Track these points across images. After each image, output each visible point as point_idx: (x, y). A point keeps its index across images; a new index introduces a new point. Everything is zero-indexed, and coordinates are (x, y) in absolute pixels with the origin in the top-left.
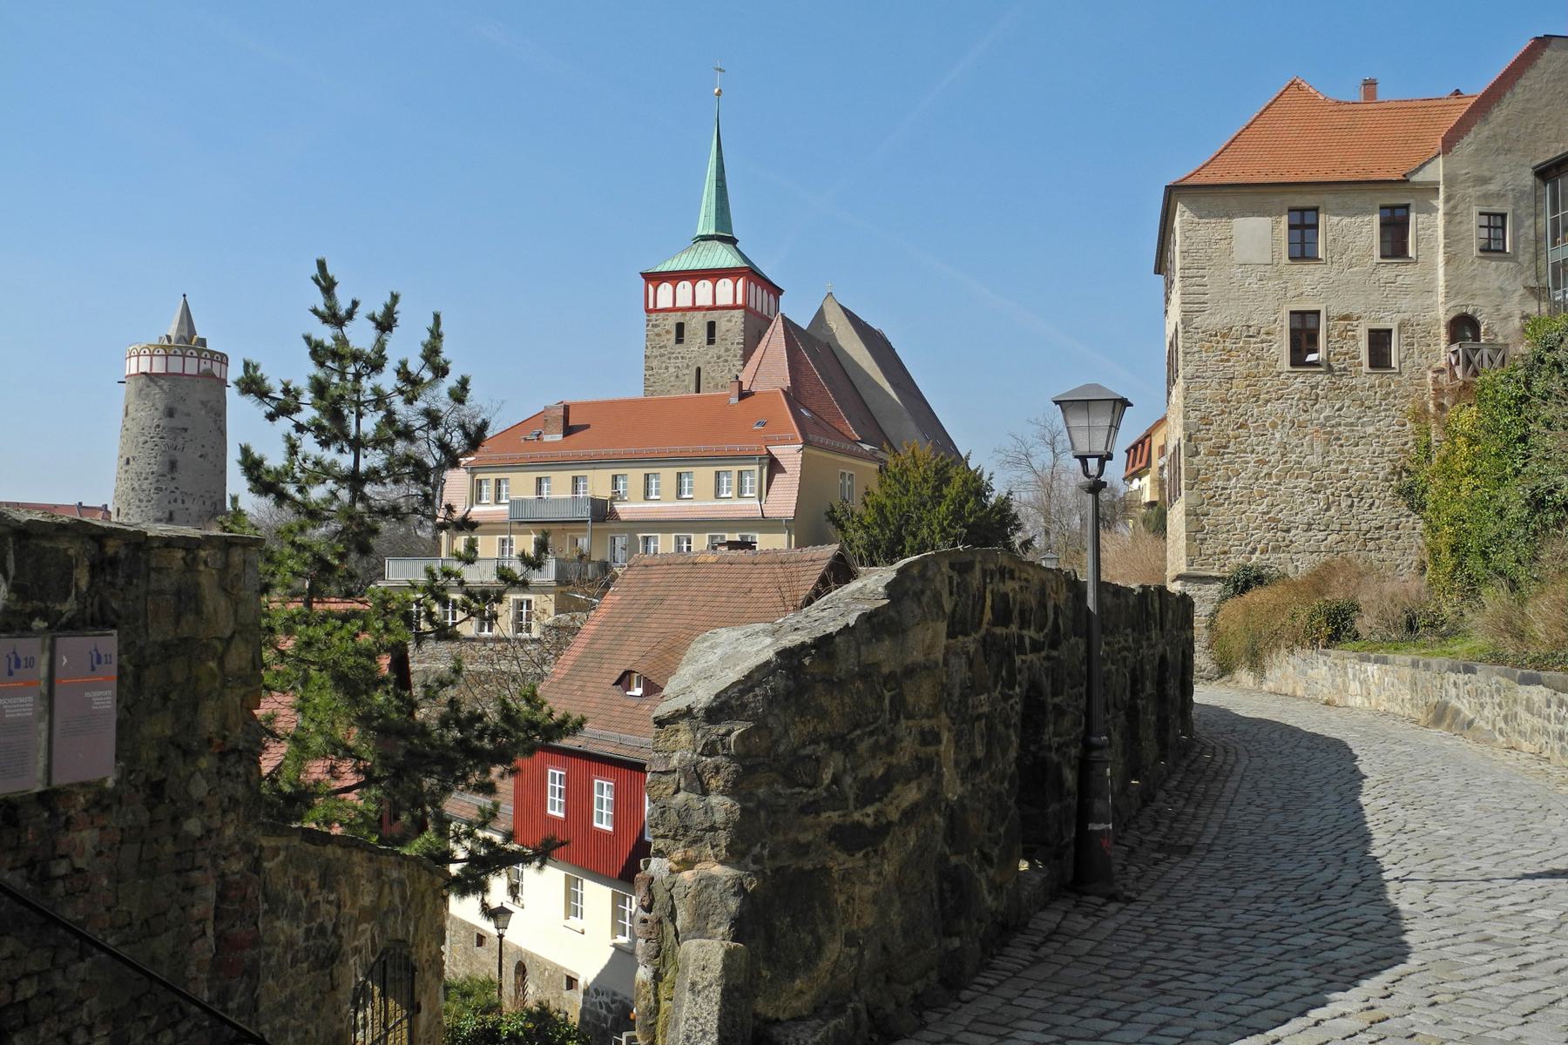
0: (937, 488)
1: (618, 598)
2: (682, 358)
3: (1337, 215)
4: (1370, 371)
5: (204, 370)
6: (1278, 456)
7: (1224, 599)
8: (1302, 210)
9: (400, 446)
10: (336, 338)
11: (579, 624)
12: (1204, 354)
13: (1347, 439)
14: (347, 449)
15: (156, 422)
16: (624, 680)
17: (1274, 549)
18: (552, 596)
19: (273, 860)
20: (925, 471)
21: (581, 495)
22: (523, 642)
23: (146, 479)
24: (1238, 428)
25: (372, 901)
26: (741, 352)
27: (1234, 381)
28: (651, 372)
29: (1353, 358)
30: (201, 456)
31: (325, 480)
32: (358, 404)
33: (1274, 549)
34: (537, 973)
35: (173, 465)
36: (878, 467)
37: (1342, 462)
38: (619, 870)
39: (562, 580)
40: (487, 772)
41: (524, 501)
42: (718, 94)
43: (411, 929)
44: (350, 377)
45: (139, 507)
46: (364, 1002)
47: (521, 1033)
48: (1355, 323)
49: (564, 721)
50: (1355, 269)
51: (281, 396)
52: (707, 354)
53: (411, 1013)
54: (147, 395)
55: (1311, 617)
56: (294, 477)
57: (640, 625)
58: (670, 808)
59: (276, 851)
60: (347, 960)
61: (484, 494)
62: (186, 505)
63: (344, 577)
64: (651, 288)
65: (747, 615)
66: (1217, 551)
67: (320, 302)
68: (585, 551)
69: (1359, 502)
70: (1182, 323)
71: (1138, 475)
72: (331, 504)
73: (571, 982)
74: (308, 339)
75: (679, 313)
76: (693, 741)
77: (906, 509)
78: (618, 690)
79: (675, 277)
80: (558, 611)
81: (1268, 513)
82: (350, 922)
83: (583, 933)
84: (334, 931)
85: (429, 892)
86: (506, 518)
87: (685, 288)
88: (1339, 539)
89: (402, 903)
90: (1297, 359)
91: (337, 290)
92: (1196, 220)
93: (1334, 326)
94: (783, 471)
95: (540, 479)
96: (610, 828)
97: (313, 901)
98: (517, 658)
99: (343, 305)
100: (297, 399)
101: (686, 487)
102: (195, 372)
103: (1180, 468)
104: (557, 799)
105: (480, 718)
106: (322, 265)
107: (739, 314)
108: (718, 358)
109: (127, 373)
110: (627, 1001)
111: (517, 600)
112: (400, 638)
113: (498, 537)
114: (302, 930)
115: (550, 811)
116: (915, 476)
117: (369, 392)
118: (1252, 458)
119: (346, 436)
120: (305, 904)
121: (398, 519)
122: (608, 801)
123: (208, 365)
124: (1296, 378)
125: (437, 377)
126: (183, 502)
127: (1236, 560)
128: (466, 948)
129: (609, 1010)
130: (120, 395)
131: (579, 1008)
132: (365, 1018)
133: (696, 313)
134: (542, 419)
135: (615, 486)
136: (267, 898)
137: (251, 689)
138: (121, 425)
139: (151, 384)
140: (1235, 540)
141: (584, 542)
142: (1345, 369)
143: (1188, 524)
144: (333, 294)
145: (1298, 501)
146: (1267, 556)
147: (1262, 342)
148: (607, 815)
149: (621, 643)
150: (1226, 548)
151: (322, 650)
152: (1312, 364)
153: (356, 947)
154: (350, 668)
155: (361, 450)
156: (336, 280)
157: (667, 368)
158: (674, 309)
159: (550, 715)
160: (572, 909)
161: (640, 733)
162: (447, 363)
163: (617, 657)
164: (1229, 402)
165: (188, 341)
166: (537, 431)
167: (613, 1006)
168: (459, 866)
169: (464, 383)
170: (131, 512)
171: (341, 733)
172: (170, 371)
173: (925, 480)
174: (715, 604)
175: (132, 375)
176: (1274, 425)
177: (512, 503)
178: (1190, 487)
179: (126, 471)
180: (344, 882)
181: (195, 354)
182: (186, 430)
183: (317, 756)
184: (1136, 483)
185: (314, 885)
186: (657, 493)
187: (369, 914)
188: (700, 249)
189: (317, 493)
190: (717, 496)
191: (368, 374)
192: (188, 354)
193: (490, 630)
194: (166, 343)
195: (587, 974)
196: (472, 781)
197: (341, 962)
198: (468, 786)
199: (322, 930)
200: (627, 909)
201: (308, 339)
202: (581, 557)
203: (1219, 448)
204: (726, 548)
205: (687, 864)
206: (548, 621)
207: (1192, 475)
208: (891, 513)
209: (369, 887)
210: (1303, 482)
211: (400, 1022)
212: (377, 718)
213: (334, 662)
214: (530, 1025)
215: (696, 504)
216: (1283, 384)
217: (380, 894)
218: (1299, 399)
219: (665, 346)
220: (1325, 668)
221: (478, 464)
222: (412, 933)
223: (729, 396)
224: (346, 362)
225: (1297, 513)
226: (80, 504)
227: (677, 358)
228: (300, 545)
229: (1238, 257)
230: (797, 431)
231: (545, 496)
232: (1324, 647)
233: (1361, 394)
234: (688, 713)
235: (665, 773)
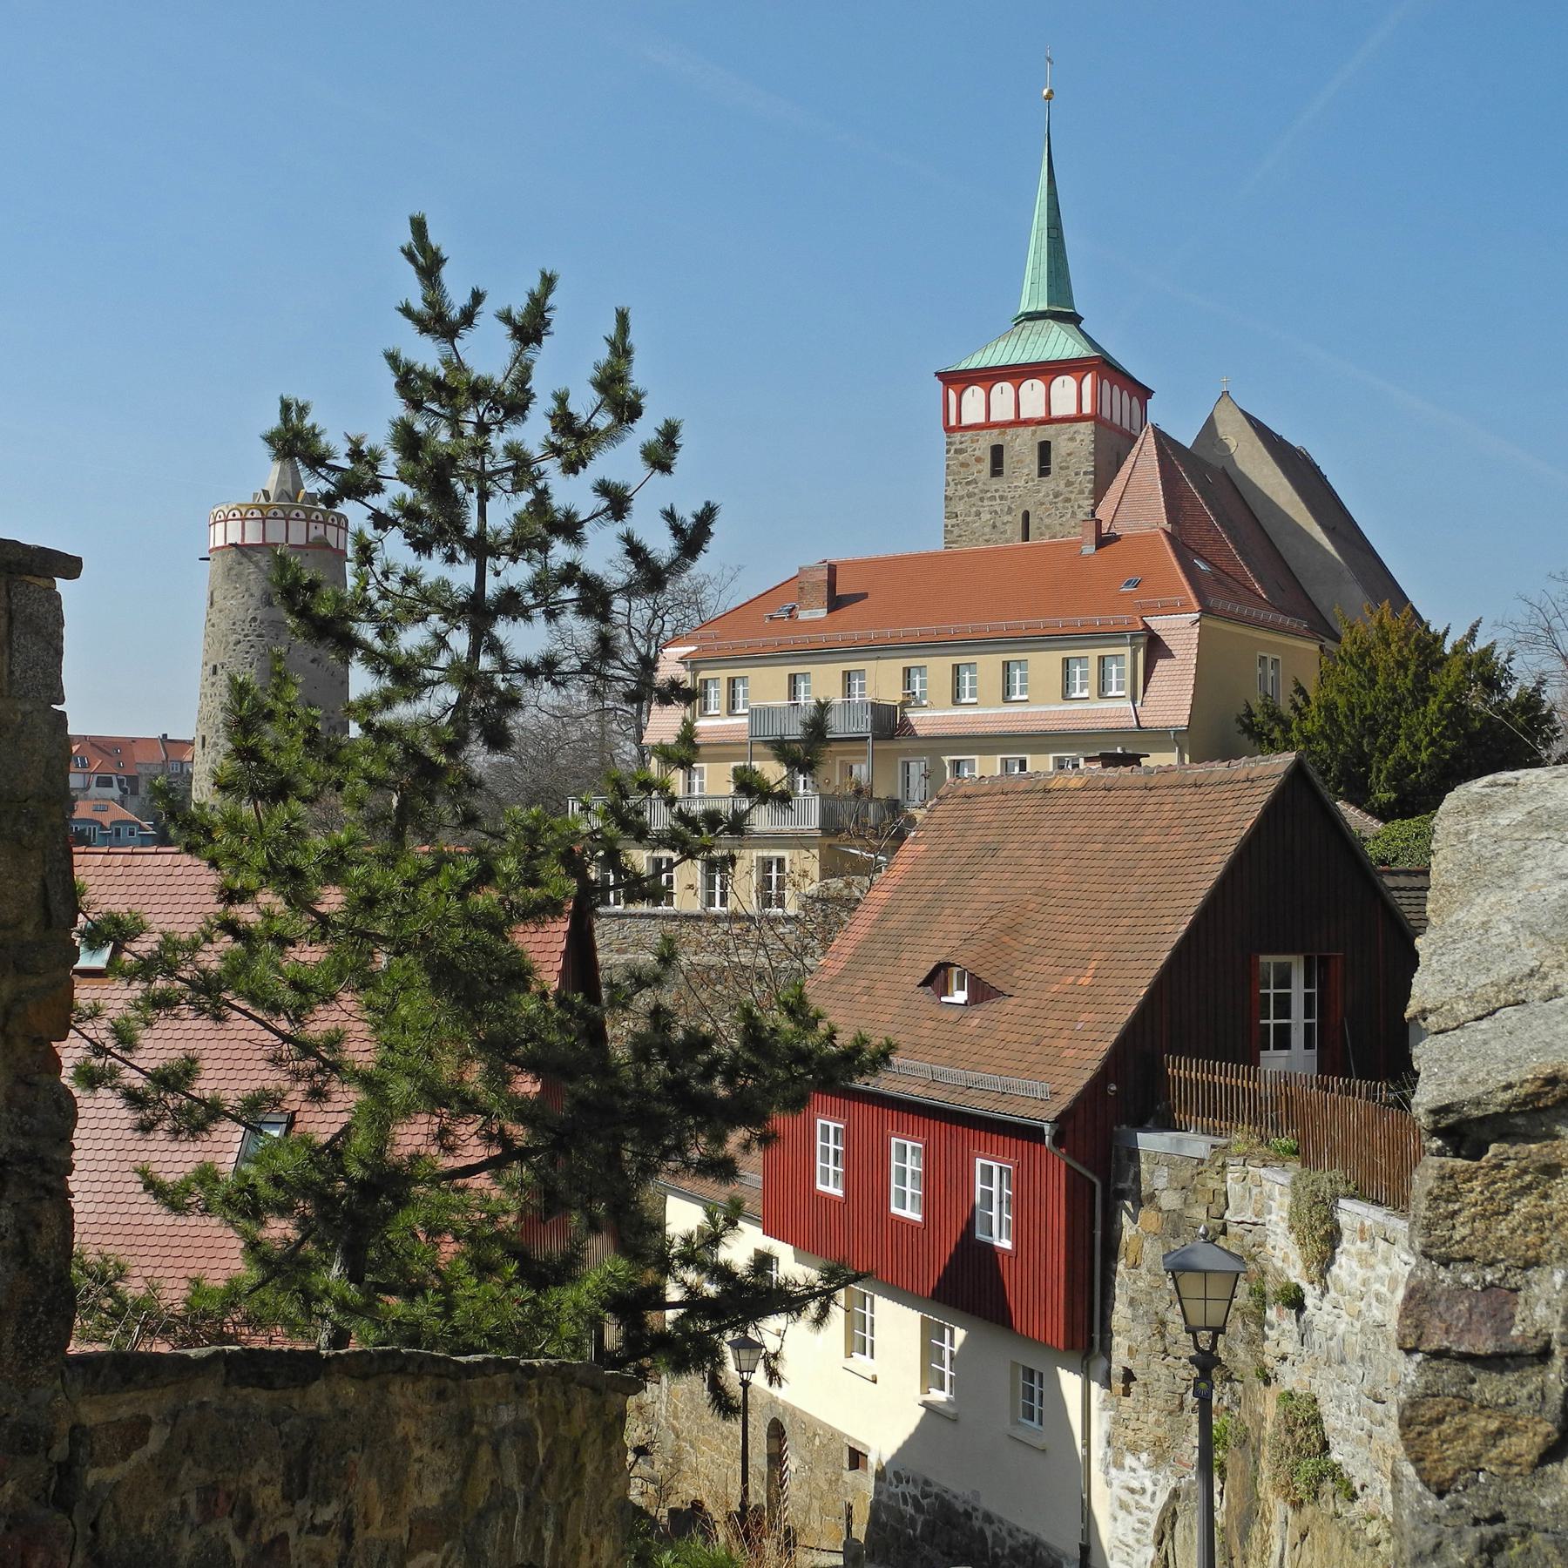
0: (1420, 678)
1: (923, 847)
2: (1001, 498)
5: (315, 538)
9: (561, 552)
10: (446, 363)
11: (857, 894)
14: (462, 555)
16: (937, 978)
18: (816, 852)
19: (125, 1456)
20: (1400, 651)
21: (857, 699)
22: (775, 920)
25: (444, 1495)
30: (313, 661)
31: (428, 614)
32: (483, 476)
34: (802, 1440)
38: (933, 1282)
39: (830, 826)
40: (720, 1139)
42: (1048, 98)
43: (548, 1535)
44: (469, 430)
51: (346, 463)
54: (239, 575)
56: (372, 610)
57: (959, 889)
58: (1525, 1530)
59: (138, 1430)
63: (458, 787)
64: (952, 395)
65: (1139, 872)
67: (414, 293)
72: (436, 656)
73: (856, 1458)
74: (392, 358)
75: (996, 431)
77: (1369, 710)
79: (988, 377)
80: (826, 873)
83: (875, 1382)
85: (592, 1435)
86: (745, 736)
87: (1003, 392)
89: (524, 1479)
91: (445, 273)
94: (1169, 655)
96: (918, 1217)
97: (266, 1538)
98: (765, 946)
99: (457, 299)
100: (374, 468)
101: (1018, 684)
102: (303, 542)
104: (831, 1167)
105: (705, 1043)
106: (419, 226)
107: (1086, 428)
108: (1056, 497)
110: (947, 1496)
111: (763, 858)
116: (1384, 658)
117: (500, 456)
119: (460, 528)
121: (555, 683)
122: (913, 1173)
123: (321, 531)
125: (620, 421)
128: (692, 1393)
129: (918, 1507)
130: (203, 577)
131: (869, 1501)
133: (1021, 430)
134: (795, 587)
137: (33, 981)
139: (244, 560)
141: (862, 771)
148: (913, 1196)
154: (458, 950)
155: (489, 560)
156: (444, 253)
157: (978, 514)
158: (988, 425)
159: (831, 1037)
160: (857, 1343)
161: (964, 1064)
162: (639, 396)
163: (922, 941)
166: (789, 605)
167: (925, 1502)
168: (670, 1315)
169: (670, 434)
171: (448, 1072)
174: (1084, 855)
175: (218, 548)
177: (753, 714)
179: (213, 684)
181: (302, 516)
185: (268, 1497)
186: (973, 693)
188: (1025, 333)
189: (412, 639)
191: (499, 423)
193: (723, 902)
194: (263, 501)
195: (883, 1444)
196: (695, 1155)
198: (688, 1165)
200: (946, 1346)
201: (392, 358)
202: (859, 792)
206: (811, 888)
208: (1346, 716)
209: (440, 1461)
212: (525, 1042)
215: (1031, 710)
219: (975, 482)
222: (549, 1543)
223: (1080, 542)
224: (461, 400)
226: (165, 736)
228: (382, 729)
235: (1498, 1362)
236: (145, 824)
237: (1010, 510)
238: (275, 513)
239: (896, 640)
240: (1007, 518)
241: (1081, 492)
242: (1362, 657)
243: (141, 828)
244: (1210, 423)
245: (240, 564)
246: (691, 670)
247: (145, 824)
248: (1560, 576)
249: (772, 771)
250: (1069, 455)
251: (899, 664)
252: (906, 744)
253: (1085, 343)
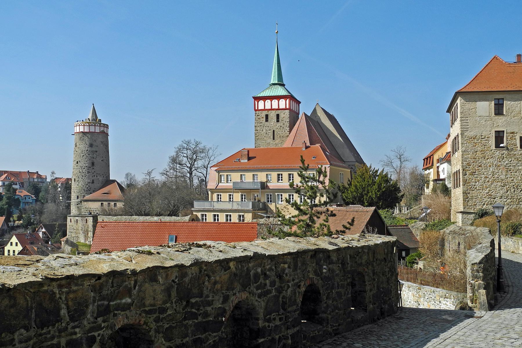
2: (268, 127)
3: (510, 101)
4: (520, 149)
5: (102, 131)
6: (491, 176)
7: (475, 219)
8: (498, 99)
12: (468, 144)
13: (513, 170)
17: (490, 204)
23: (84, 169)
24: (479, 167)
27: (477, 152)
28: (257, 132)
29: (515, 145)
30: (102, 161)
33: (490, 204)
35: (93, 164)
36: (350, 171)
37: (511, 178)
42: (277, 33)
45: (82, 178)
48: (515, 135)
50: (516, 118)
52: (277, 126)
54: (83, 139)
55: (507, 228)
61: (222, 179)
62: (98, 178)
66: (473, 204)
69: (517, 190)
70: (461, 134)
71: (429, 168)
75: (266, 111)
76: (477, 266)
79: (264, 98)
80: (253, 218)
81: (488, 193)
86: (232, 187)
87: (268, 102)
88: (511, 201)
90: (497, 146)
92: (465, 102)
93: (509, 135)
102: (99, 132)
103: (459, 178)
107: (287, 112)
109: (75, 132)
111: (239, 215)
113: (228, 194)
118: (482, 176)
124: (497, 152)
126: (97, 177)
127: (478, 207)
130: (73, 140)
139: (84, 136)
140: (478, 201)
142: (512, 149)
143: (463, 196)
145: (498, 189)
146: (488, 206)
147: (486, 140)
150: (475, 204)
152: (502, 147)
157: (263, 130)
158: (265, 110)
164: (476, 159)
165: (95, 121)
166: (238, 158)
170: (79, 180)
172: (90, 131)
176: (490, 166)
178: (464, 185)
181: (99, 125)
182: (97, 151)
184: (427, 172)
188: (273, 88)
192: (96, 125)
194: (88, 121)
203: (473, 173)
205: (477, 281)
207: (465, 181)
208: (359, 188)
210: (499, 184)
216: (493, 153)
218: (498, 158)
219: (262, 123)
220: (511, 242)
225: (497, 193)
226: (28, 171)
227: (266, 127)
229: (478, 114)
230: (327, 160)
232: (511, 236)
233: (517, 156)
234: (476, 263)
236: (32, 196)
237: (270, 130)
238: (92, 124)
239: (264, 168)
240: (269, 132)
241: (286, 126)
243: (32, 197)
244: (315, 110)
245: (83, 136)
246: (218, 173)
247: (32, 196)
248: (393, 151)
249: (348, 226)
250: (284, 117)
251: (265, 173)
252: (267, 190)
253: (287, 91)
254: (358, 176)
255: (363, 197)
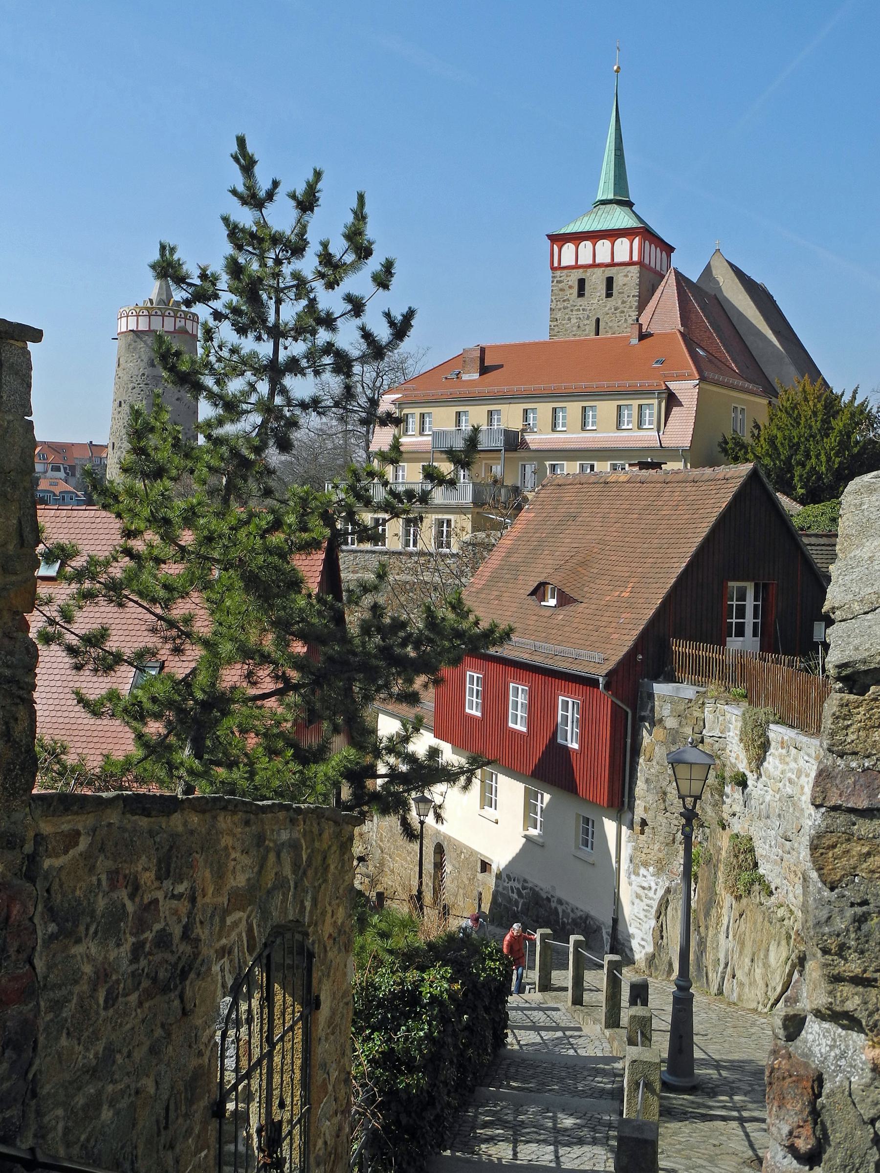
1: (533, 515)
2: (583, 310)
10: (257, 223)
11: (493, 541)
14: (265, 337)
15: (142, 371)
16: (539, 591)
18: (470, 516)
19: (66, 852)
20: (815, 406)
25: (249, 880)
26: (636, 304)
28: (555, 323)
30: (177, 399)
31: (245, 371)
32: (278, 290)
38: (532, 767)
39: (478, 502)
40: (410, 681)
41: (444, 433)
42: (617, 71)
43: (308, 904)
46: (249, 990)
47: (445, 996)
49: (491, 631)
51: (197, 282)
53: (306, 1012)
54: (135, 349)
56: (212, 369)
57: (553, 540)
59: (73, 838)
60: (210, 969)
64: (556, 248)
67: (239, 182)
68: (499, 476)
73: (485, 866)
74: (226, 220)
75: (581, 270)
77: (796, 440)
78: (532, 601)
79: (577, 238)
80: (475, 529)
82: (212, 916)
84: (186, 935)
85: (334, 848)
87: (586, 247)
89: (294, 872)
91: (257, 169)
95: (459, 413)
96: (524, 729)
97: (146, 901)
99: (263, 185)
100: (214, 285)
101: (590, 420)
102: (172, 329)
104: (475, 699)
105: (403, 625)
106: (241, 142)
107: (635, 269)
110: (537, 889)
111: (439, 519)
112: (314, 535)
114: (126, 948)
115: (468, 710)
116: (806, 410)
117: (288, 278)
119: (264, 321)
120: (130, 907)
121: (319, 413)
123: (183, 323)
125: (360, 258)
128: (391, 827)
132: (249, 1011)
134: (461, 360)
135: (526, 419)
136: (52, 913)
138: (114, 374)
139: (138, 340)
141: (497, 469)
144: (252, 173)
148: (522, 717)
149: (535, 556)
151: (227, 547)
153: (223, 948)
154: (261, 568)
155: (281, 340)
156: (256, 158)
157: (569, 319)
158: (577, 267)
159: (476, 623)
162: (371, 243)
163: (531, 569)
166: (457, 371)
167: (524, 892)
168: (380, 782)
169: (389, 267)
173: (815, 413)
177: (435, 435)
180: (201, 863)
181: (172, 314)
183: (230, 661)
185: (147, 878)
186: (564, 425)
187: (239, 899)
188: (600, 213)
189: (235, 386)
190: (618, 428)
192: (167, 314)
193: (415, 544)
194: (149, 305)
195: (500, 859)
196: (395, 690)
197: (198, 974)
199: (163, 941)
200: (539, 803)
201: (226, 220)
202: (495, 481)
204: (637, 468)
206: (467, 537)
208: (782, 444)
209: (246, 860)
211: (291, 1028)
212: (299, 622)
213: (240, 560)
214: (457, 987)
217: (262, 867)
219: (568, 300)
221: (405, 400)
222: (308, 909)
224: (266, 245)
226: (91, 442)
227: (578, 310)
228: (217, 438)
231: (464, 428)
236: (79, 493)
240: (586, 322)
241: (631, 307)
242: (793, 409)
243: (77, 496)
247: (79, 493)
253: (635, 219)
254: (781, 411)
255: (790, 469)
